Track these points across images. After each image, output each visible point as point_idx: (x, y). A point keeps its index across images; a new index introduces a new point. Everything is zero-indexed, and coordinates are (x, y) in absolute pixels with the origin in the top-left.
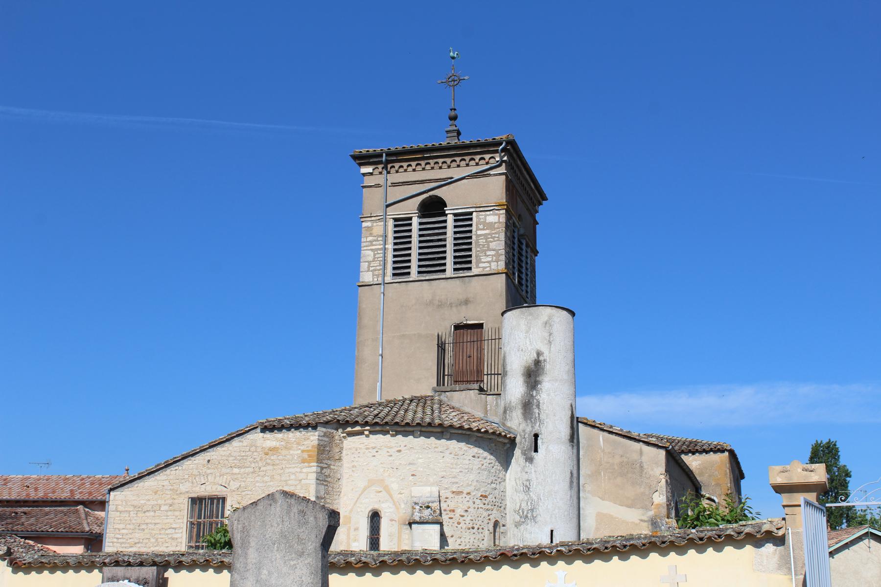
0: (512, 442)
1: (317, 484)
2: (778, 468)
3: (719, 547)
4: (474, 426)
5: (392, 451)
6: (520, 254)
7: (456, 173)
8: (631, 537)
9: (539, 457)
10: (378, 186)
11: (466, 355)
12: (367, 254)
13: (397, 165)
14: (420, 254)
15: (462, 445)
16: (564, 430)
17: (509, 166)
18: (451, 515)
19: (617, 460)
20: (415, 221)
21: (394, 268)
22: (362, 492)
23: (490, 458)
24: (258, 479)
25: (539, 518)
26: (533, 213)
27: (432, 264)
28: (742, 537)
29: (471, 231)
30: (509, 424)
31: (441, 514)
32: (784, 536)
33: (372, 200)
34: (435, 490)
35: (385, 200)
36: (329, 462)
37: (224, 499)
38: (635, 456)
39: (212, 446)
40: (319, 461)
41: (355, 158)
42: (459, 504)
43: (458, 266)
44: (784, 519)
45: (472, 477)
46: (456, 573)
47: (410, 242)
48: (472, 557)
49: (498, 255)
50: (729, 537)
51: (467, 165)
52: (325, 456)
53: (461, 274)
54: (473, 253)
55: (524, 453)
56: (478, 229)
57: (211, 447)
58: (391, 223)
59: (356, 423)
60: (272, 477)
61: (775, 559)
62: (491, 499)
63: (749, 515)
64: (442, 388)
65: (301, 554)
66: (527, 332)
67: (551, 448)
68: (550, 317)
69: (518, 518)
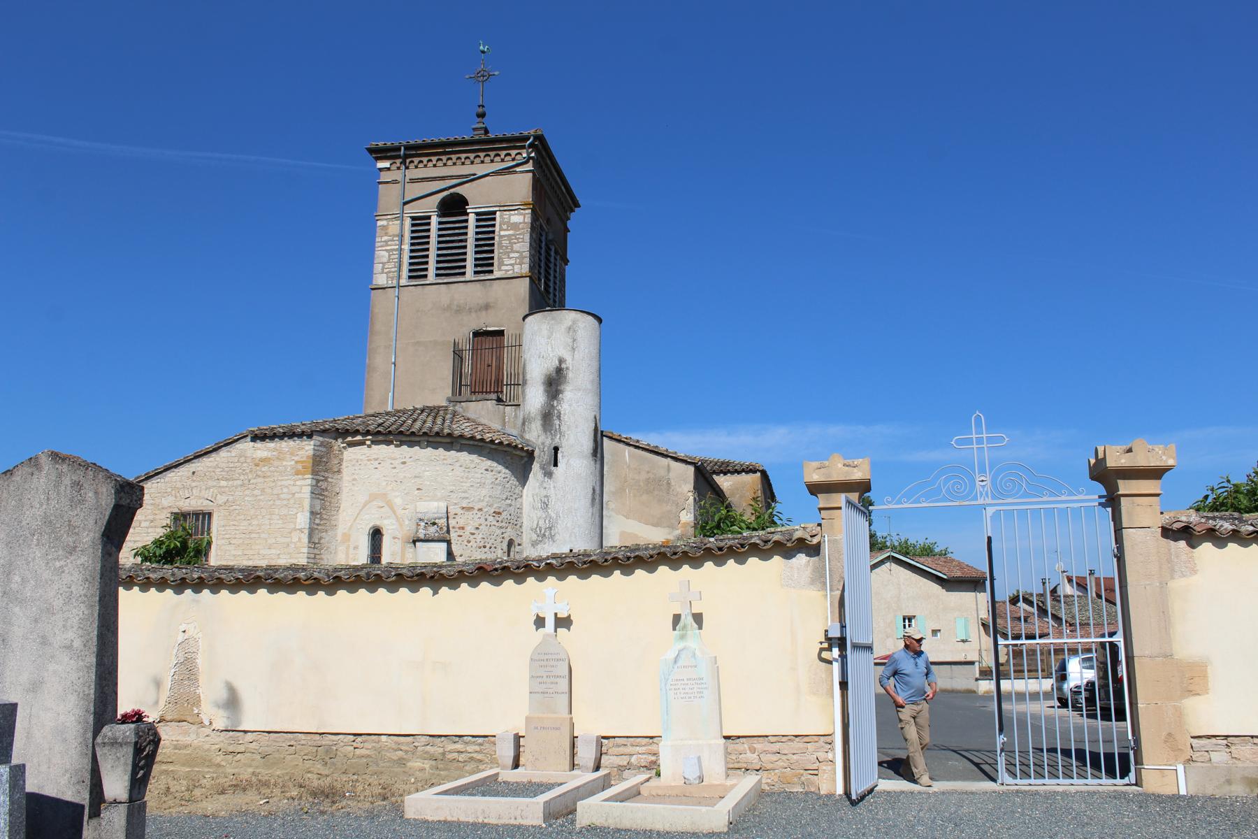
0: (530, 455)
1: (312, 498)
2: (815, 464)
3: (741, 558)
4: (488, 437)
5: (396, 463)
6: (548, 260)
7: (479, 169)
8: (637, 548)
9: (558, 472)
10: (395, 182)
11: (485, 363)
12: (382, 255)
13: (416, 160)
14: (438, 256)
15: (474, 457)
16: (587, 444)
17: (537, 163)
18: (460, 532)
19: (644, 476)
20: (434, 220)
21: (410, 271)
22: (365, 506)
23: (505, 472)
24: (247, 492)
25: (557, 537)
26: (564, 220)
27: (451, 267)
28: (769, 545)
29: (493, 232)
30: (527, 436)
31: (448, 531)
32: (819, 544)
33: (389, 197)
34: (443, 505)
35: (401, 200)
36: (326, 474)
37: (210, 514)
38: (662, 472)
39: (197, 457)
40: (315, 473)
41: (371, 151)
42: (469, 521)
43: (479, 269)
44: (820, 525)
45: (484, 492)
46: (426, 591)
47: (428, 243)
48: (443, 571)
49: (522, 257)
50: (755, 545)
51: (492, 161)
52: (321, 468)
53: (482, 277)
54: (496, 255)
55: (542, 468)
56: (501, 229)
57: (196, 457)
58: (408, 222)
59: (357, 432)
60: (263, 490)
61: (808, 572)
62: (507, 517)
63: (779, 522)
64: (458, 398)
65: (72, 550)
66: (549, 338)
67: (571, 462)
68: (574, 322)
69: (534, 537)
